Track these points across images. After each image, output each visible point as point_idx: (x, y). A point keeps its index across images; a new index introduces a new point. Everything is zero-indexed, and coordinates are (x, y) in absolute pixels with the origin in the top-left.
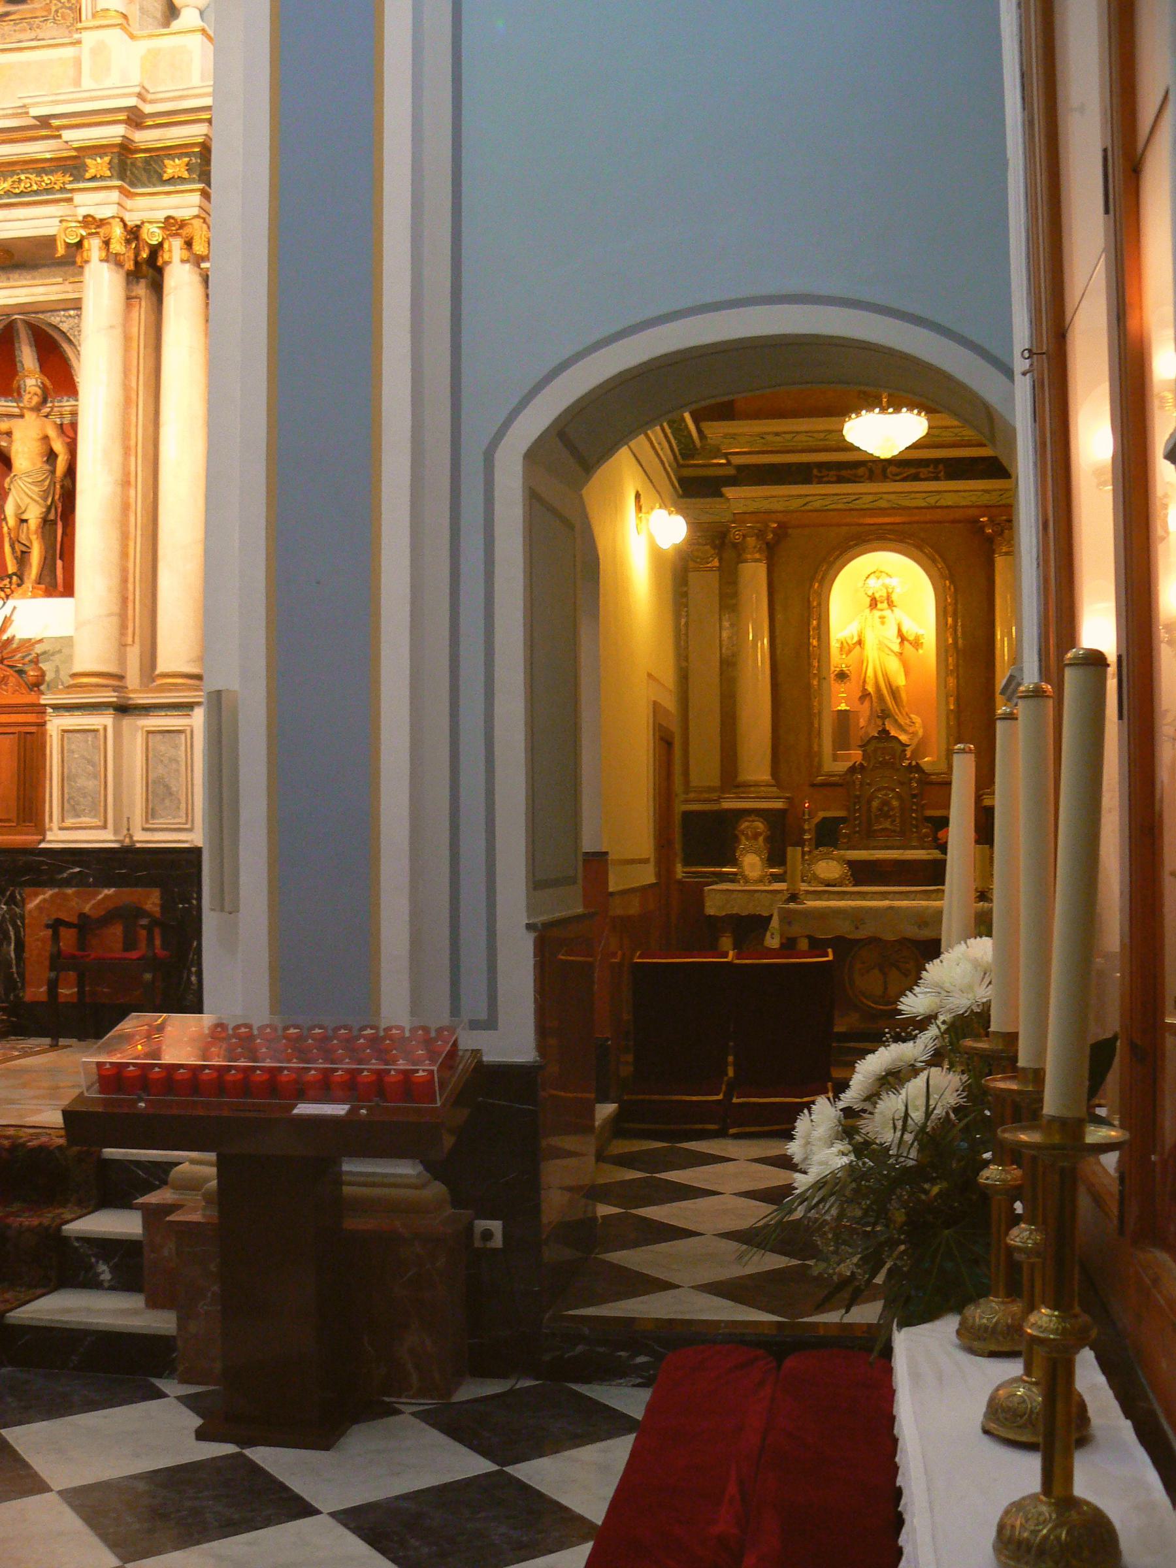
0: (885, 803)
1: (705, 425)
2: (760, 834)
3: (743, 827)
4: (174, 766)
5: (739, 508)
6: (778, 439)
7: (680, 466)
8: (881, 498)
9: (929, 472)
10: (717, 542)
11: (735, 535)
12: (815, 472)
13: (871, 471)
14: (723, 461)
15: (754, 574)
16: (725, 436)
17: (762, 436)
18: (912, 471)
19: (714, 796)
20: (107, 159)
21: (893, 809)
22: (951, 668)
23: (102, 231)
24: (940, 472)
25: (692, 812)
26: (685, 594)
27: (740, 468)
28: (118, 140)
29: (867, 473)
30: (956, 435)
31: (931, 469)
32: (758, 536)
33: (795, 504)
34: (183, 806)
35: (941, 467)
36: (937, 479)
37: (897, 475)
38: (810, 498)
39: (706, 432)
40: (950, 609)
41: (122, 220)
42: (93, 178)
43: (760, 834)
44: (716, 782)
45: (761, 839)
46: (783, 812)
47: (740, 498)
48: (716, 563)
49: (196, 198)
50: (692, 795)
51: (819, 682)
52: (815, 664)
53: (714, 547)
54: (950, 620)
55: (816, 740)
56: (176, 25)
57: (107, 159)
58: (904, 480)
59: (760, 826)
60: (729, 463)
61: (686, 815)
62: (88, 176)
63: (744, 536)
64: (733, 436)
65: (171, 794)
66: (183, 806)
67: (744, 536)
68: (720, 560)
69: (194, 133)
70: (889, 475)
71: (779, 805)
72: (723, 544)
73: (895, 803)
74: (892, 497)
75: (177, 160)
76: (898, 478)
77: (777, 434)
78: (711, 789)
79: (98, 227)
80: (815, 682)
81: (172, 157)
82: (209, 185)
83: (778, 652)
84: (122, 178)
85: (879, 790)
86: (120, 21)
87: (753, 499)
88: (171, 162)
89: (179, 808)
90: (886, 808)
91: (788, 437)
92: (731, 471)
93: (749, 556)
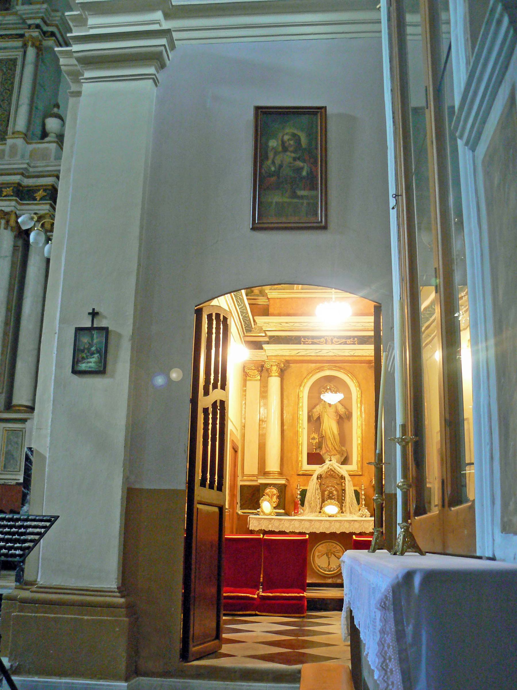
0: (331, 493)
1: (255, 318)
2: (274, 495)
3: (267, 492)
4: (16, 446)
5: (269, 353)
6: (287, 325)
7: (245, 336)
8: (330, 351)
9: (351, 341)
10: (260, 369)
11: (267, 366)
12: (302, 339)
13: (326, 340)
14: (264, 335)
15: (274, 382)
16: (265, 323)
17: (280, 323)
18: (344, 340)
19: (255, 478)
20: (11, 188)
21: (334, 496)
22: (359, 425)
23: (6, 217)
24: (355, 341)
25: (245, 486)
26: (245, 391)
27: (271, 337)
28: (17, 181)
29: (325, 340)
30: (363, 326)
31: (352, 340)
32: (277, 366)
33: (294, 353)
34: (18, 464)
35: (356, 339)
36: (354, 344)
37: (337, 342)
38: (300, 351)
39: (257, 321)
40: (359, 400)
41: (16, 213)
42: (5, 196)
43: (274, 495)
44: (256, 472)
45: (275, 497)
46: (285, 486)
47: (271, 349)
48: (259, 378)
49: (48, 207)
50: (245, 478)
51: (302, 430)
52: (301, 422)
53: (258, 371)
54: (359, 405)
55: (300, 456)
56: (47, 139)
57: (11, 188)
58: (340, 344)
59: (275, 491)
60: (266, 336)
61: (241, 486)
62: (3, 195)
63: (271, 366)
64: (268, 323)
65: (14, 459)
66: (18, 464)
67: (271, 366)
68: (261, 376)
69: (48, 181)
70: (334, 342)
71: (283, 482)
72: (262, 370)
73: (335, 493)
74: (334, 351)
75: (8, 189)
76: (338, 343)
77: (287, 323)
78: (253, 476)
79: (5, 215)
80: (301, 430)
81: (5, 188)
82: (55, 202)
83: (284, 417)
84: (17, 196)
85: (328, 487)
86: (24, 136)
87: (276, 350)
88: (6, 190)
89: (17, 465)
90: (331, 495)
91: (292, 324)
92: (267, 339)
93: (273, 374)
